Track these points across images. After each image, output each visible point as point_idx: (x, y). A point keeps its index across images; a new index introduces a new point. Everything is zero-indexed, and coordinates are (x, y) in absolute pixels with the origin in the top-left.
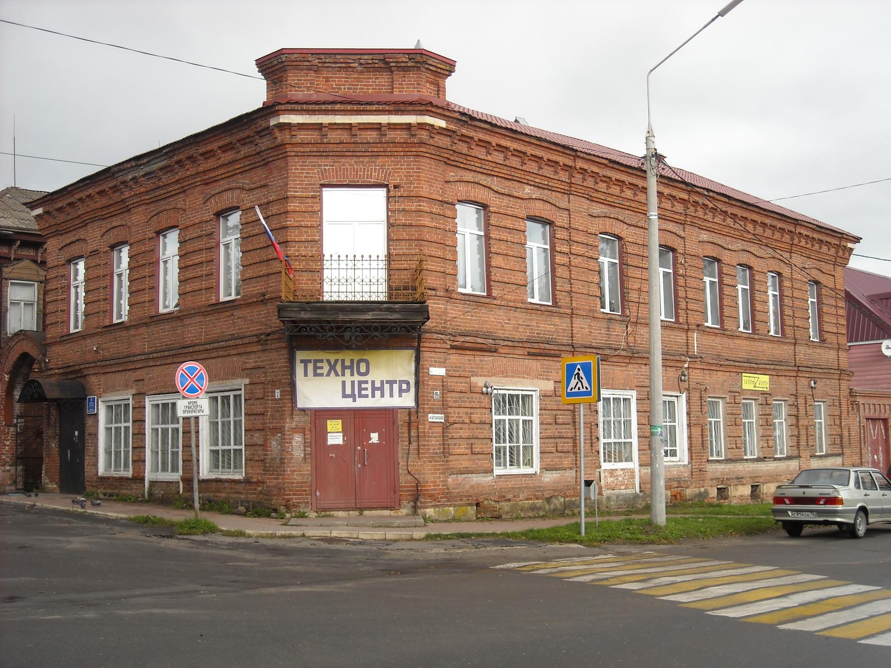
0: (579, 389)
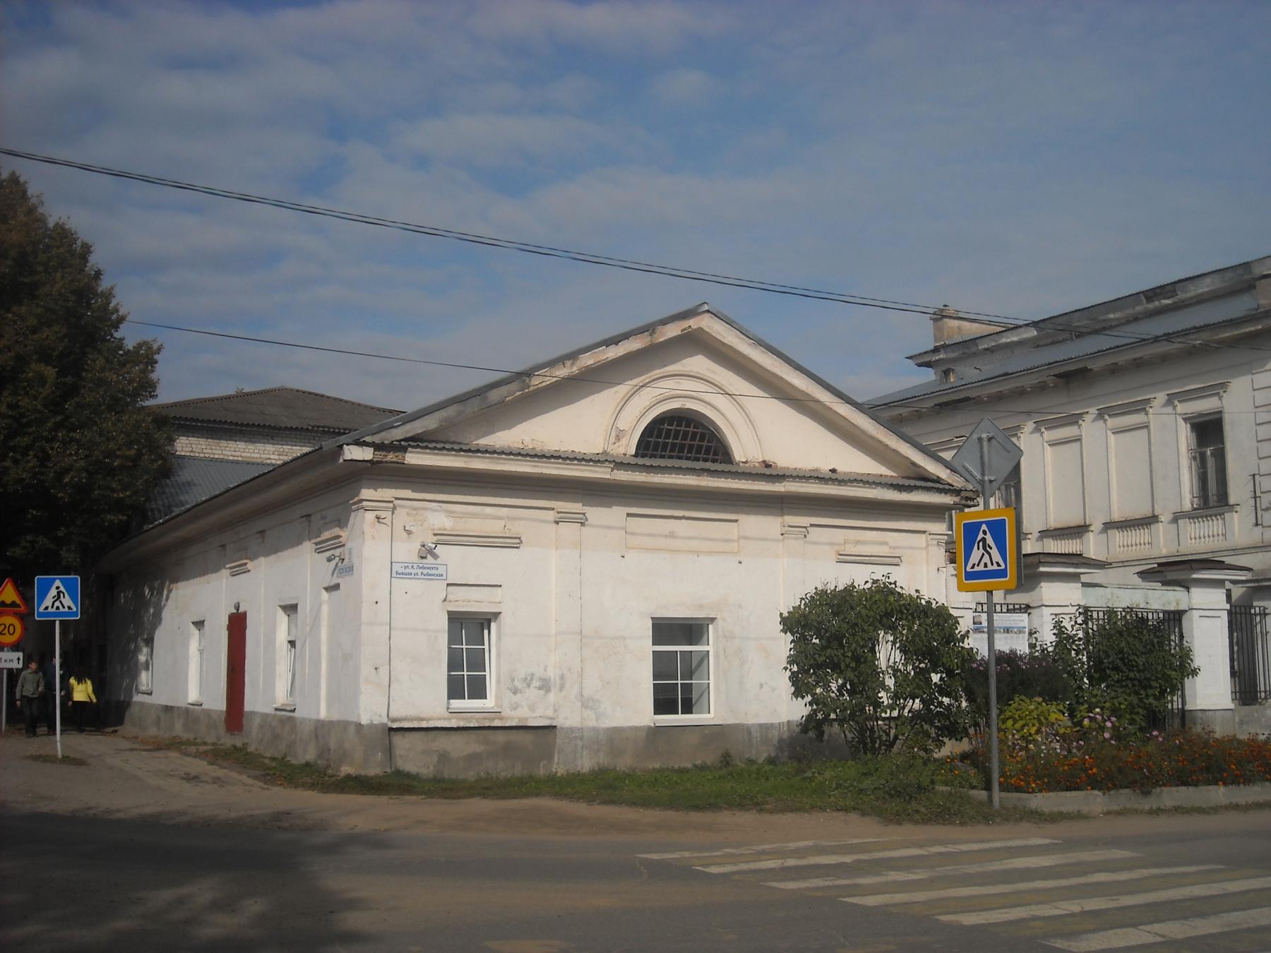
0: (986, 565)
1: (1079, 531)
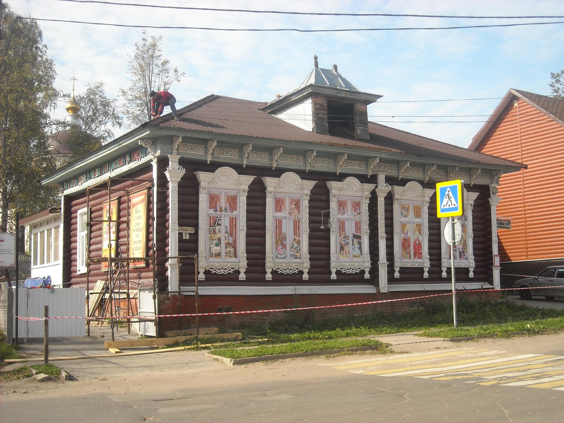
0: (449, 206)
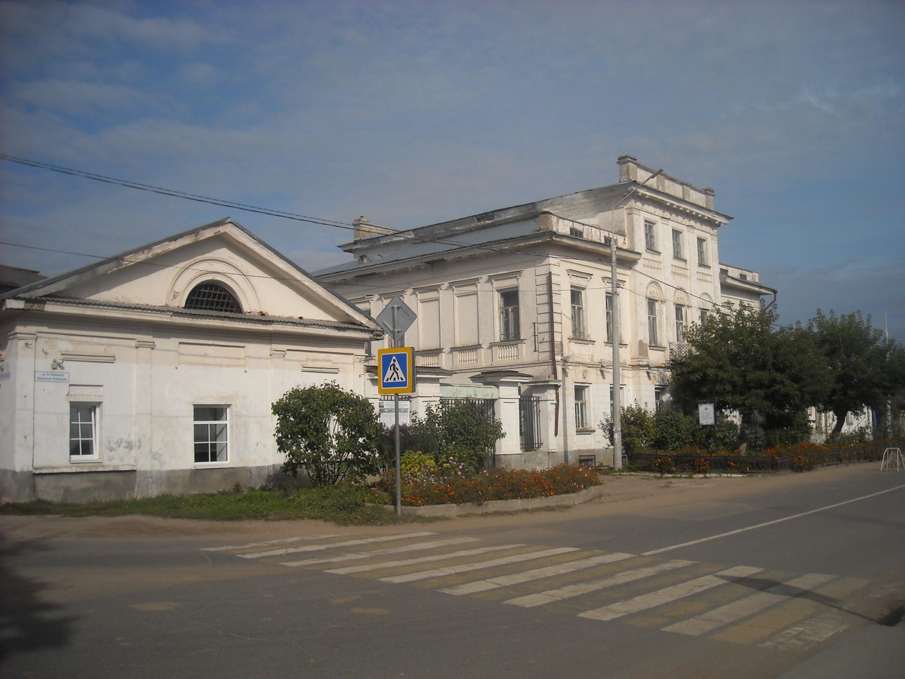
0: (395, 379)
1: (436, 352)
